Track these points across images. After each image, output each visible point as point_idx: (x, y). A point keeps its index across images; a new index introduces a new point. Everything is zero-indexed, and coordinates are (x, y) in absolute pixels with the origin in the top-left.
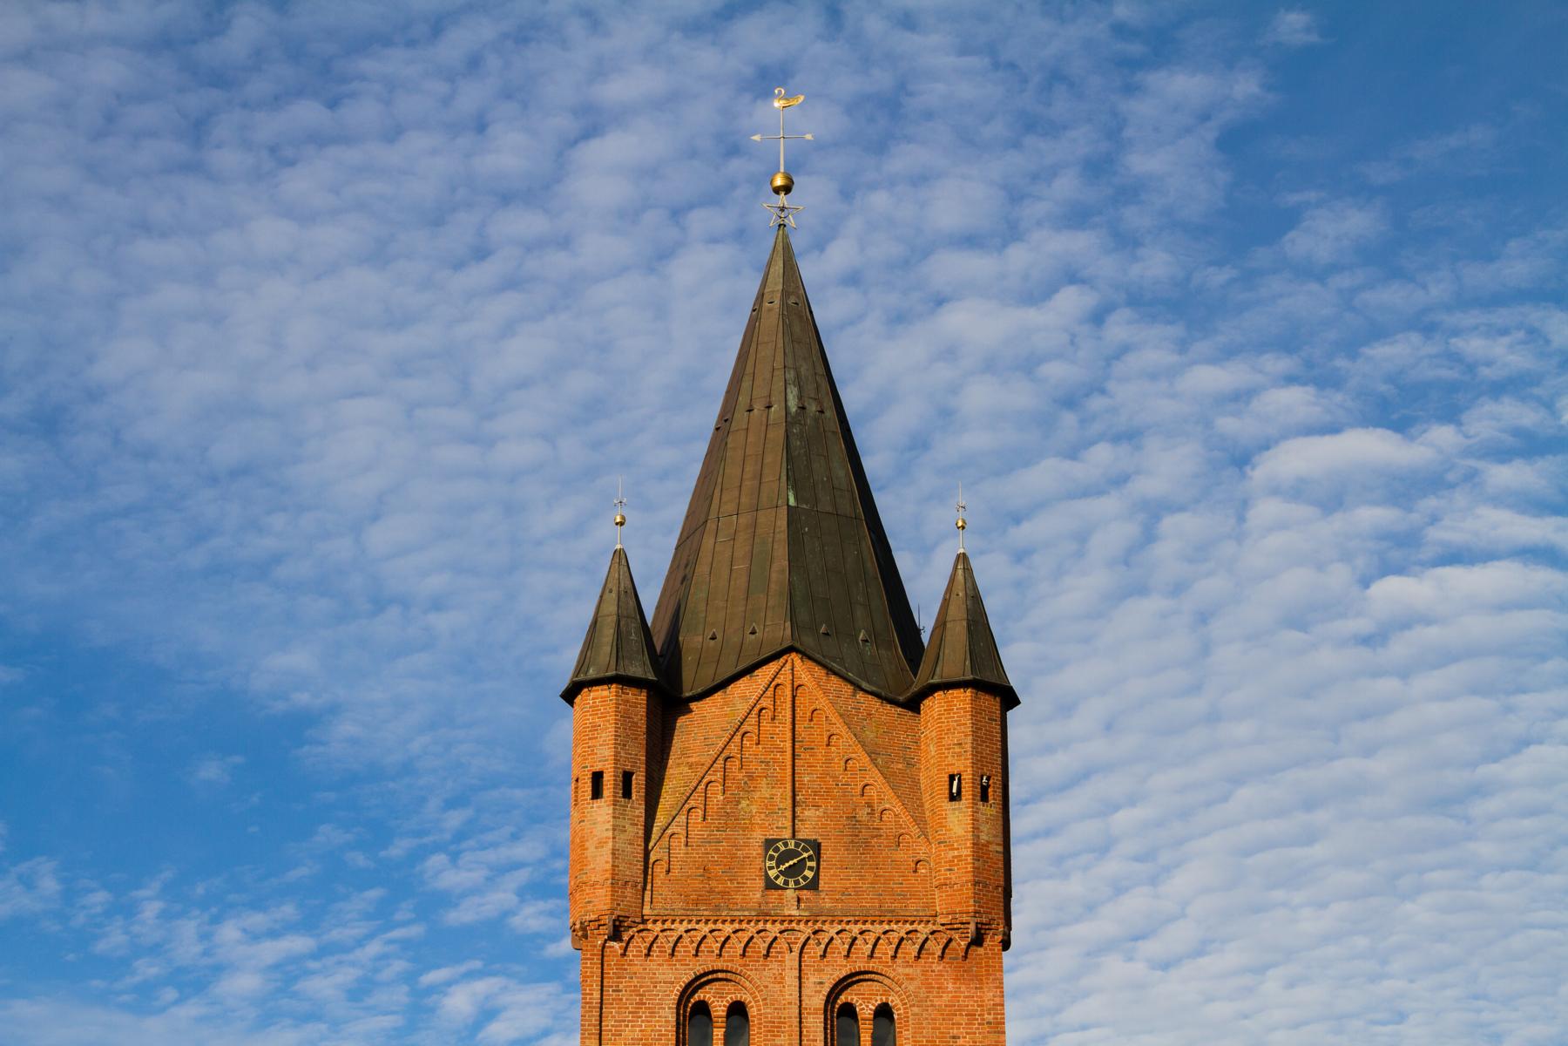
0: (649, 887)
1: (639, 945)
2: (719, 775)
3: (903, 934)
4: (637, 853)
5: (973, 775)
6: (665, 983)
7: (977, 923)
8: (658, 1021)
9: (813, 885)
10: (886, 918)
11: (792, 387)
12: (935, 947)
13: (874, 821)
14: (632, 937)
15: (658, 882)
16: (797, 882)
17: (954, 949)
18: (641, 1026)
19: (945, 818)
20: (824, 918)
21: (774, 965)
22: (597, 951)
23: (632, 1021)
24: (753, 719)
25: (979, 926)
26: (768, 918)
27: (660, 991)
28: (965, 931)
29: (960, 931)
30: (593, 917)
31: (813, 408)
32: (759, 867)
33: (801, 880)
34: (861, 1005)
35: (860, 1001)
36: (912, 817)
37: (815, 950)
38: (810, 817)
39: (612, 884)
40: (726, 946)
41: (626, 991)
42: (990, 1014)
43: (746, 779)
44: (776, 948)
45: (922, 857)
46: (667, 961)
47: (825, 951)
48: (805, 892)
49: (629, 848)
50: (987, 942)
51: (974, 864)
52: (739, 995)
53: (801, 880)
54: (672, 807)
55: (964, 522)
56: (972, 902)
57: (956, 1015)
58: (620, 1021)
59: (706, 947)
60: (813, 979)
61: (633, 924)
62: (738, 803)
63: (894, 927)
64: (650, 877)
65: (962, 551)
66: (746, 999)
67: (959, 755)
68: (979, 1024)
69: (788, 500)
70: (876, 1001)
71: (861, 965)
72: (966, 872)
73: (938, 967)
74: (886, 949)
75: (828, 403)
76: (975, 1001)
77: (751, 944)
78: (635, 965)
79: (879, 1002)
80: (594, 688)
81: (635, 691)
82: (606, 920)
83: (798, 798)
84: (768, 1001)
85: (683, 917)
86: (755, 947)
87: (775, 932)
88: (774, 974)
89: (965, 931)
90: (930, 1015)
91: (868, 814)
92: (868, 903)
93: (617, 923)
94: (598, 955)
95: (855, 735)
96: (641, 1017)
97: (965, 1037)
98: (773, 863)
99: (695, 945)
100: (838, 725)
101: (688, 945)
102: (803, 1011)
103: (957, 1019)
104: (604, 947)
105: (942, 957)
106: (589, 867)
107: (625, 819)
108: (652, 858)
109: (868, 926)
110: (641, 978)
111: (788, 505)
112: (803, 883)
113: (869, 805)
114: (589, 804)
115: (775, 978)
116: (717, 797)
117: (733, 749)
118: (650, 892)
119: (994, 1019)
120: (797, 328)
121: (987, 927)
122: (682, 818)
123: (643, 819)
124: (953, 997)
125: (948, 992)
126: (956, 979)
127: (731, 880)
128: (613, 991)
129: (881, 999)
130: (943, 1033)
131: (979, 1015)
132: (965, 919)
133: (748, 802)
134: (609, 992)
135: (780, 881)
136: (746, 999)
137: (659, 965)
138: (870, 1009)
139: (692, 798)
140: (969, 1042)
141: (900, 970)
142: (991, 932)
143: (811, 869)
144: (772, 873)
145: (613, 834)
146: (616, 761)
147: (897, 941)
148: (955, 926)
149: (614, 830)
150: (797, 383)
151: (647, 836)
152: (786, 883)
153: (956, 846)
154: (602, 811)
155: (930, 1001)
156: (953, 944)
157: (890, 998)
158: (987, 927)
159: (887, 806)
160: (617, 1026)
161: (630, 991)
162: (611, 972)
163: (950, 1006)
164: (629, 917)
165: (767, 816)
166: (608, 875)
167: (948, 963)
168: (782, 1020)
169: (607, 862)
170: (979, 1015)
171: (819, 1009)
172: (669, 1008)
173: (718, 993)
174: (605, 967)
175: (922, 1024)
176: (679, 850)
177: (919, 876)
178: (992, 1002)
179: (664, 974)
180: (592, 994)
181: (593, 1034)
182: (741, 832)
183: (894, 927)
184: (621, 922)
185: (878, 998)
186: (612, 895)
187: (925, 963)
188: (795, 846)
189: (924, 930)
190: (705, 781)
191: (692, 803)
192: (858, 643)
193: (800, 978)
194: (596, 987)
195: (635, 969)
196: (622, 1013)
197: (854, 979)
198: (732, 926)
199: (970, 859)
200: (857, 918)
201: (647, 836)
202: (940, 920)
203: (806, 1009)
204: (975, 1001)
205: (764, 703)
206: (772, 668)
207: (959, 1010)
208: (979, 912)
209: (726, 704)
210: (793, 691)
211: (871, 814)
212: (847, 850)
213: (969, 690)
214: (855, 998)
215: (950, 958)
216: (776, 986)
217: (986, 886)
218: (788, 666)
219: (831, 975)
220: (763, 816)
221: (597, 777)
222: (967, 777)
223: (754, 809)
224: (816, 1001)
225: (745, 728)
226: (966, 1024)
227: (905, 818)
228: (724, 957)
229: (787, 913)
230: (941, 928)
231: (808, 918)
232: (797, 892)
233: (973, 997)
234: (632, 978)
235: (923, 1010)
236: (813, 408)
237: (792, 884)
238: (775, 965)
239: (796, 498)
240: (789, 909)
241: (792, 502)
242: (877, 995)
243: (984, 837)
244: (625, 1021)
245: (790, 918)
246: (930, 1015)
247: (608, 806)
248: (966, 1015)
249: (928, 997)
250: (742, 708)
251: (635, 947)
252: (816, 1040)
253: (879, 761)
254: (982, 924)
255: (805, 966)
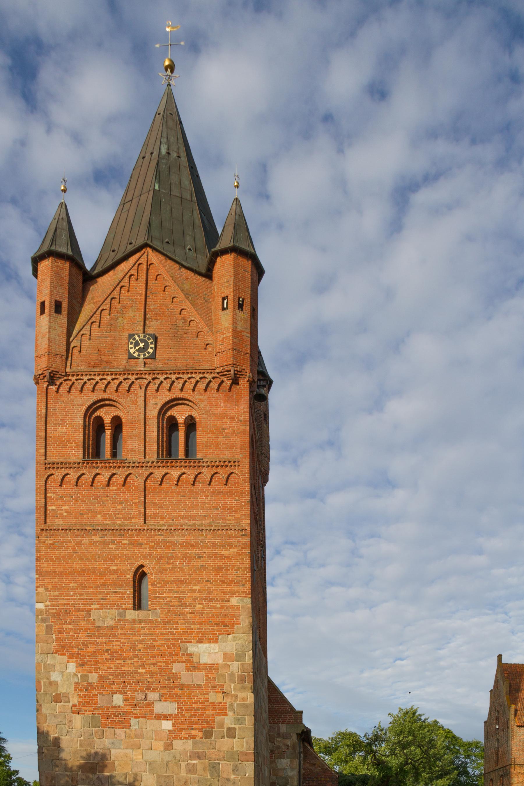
0: (70, 359)
1: (65, 387)
2: (107, 307)
3: (198, 378)
4: (63, 341)
5: (234, 296)
6: (78, 405)
7: (235, 370)
8: (75, 424)
9: (153, 356)
10: (189, 371)
11: (164, 145)
12: (214, 385)
13: (186, 326)
14: (61, 383)
15: (74, 357)
16: (144, 355)
17: (224, 387)
18: (66, 426)
19: (220, 319)
20: (158, 372)
21: (132, 396)
22: (44, 390)
23: (62, 424)
24: (126, 279)
25: (236, 372)
26: (129, 372)
27: (76, 409)
28: (229, 376)
29: (227, 376)
30: (40, 372)
31: (174, 155)
32: (126, 349)
33: (146, 354)
34: (178, 416)
35: (178, 415)
36: (205, 323)
37: (153, 387)
38: (153, 325)
39: (48, 354)
40: (109, 387)
41: (59, 410)
42: (242, 417)
43: (121, 308)
44: (134, 387)
45: (209, 342)
46: (79, 395)
47: (158, 388)
48: (149, 360)
49: (58, 338)
50: (241, 382)
51: (233, 340)
52: (117, 413)
53: (146, 354)
54: (83, 321)
55: (238, 183)
56: (231, 359)
57: (225, 418)
58: (56, 424)
59: (98, 388)
60: (152, 402)
61: (61, 377)
62: (117, 319)
63: (194, 375)
64: (70, 354)
65: (236, 197)
66: (120, 415)
67: (227, 287)
68: (236, 422)
69: (155, 186)
70: (186, 414)
71: (177, 395)
72: (229, 345)
73: (216, 395)
74: (189, 386)
75: (182, 148)
76: (234, 411)
77: (121, 386)
78: (63, 397)
79: (187, 415)
80: (42, 262)
81: (63, 262)
82: (47, 373)
83: (147, 316)
84: (129, 413)
85: (87, 373)
86: (123, 387)
87: (133, 379)
88: (133, 400)
89: (229, 376)
90: (212, 418)
91: (183, 323)
92: (180, 364)
93: (52, 375)
94: (44, 392)
95: (178, 286)
96: (66, 422)
97: (229, 429)
98: (132, 346)
99: (92, 386)
100: (169, 281)
101: (89, 386)
102: (147, 418)
103: (225, 420)
104: (47, 388)
105: (218, 390)
106: (39, 349)
107: (56, 323)
108: (72, 345)
109: (181, 376)
110: (66, 403)
111: (154, 189)
112: (147, 355)
113: (184, 319)
114: (39, 318)
115: (133, 402)
116: (106, 317)
117: (116, 294)
118: (70, 361)
119: (243, 419)
120: (170, 123)
121: (240, 373)
122: (88, 327)
123: (66, 325)
124: (223, 410)
125: (221, 407)
126: (225, 401)
127: (112, 355)
128: (53, 410)
129: (189, 414)
130: (218, 427)
131: (236, 418)
132: (228, 368)
133: (122, 319)
134: (50, 410)
135: (136, 355)
136: (120, 415)
137: (75, 397)
138: (183, 419)
139: (93, 317)
140: (231, 431)
141: (197, 397)
142: (243, 377)
143: (152, 348)
144: (132, 351)
145: (49, 330)
146: (51, 294)
147: (195, 382)
148: (224, 373)
149: (49, 328)
150: (167, 144)
151: (69, 334)
152: (139, 355)
153: (224, 332)
154: (45, 320)
155: (212, 412)
156: (224, 384)
157: (193, 413)
158: (240, 373)
159: (193, 319)
160: (54, 426)
161: (61, 410)
162: (50, 401)
163: (222, 414)
164: (58, 372)
165: (131, 325)
166: (47, 351)
167: (221, 393)
168: (136, 422)
169: (46, 344)
170: (236, 418)
171: (155, 417)
172: (80, 417)
173: (107, 412)
174: (49, 398)
175: (207, 423)
176: (86, 342)
177: (208, 352)
178: (242, 411)
179: (77, 401)
180: (42, 411)
181: (42, 430)
182: (118, 333)
183: (194, 375)
184: (54, 374)
185: (187, 413)
186: (48, 360)
187: (210, 393)
188: (144, 337)
189: (209, 377)
190: (100, 309)
191: (93, 319)
192: (185, 250)
193: (145, 401)
194: (44, 407)
195: (63, 399)
196: (57, 420)
197: (174, 403)
198: (111, 377)
199: (231, 338)
200: (174, 371)
201: (69, 334)
202: (218, 370)
203: (149, 416)
204: (234, 411)
205: (133, 272)
206: (137, 255)
207: (227, 416)
208: (236, 365)
209: (114, 275)
210: (147, 266)
211: (184, 323)
212: (171, 340)
213: (233, 254)
214: (175, 413)
215: (223, 391)
216: (134, 406)
217: (239, 352)
218: (145, 254)
219: (161, 400)
220: (129, 325)
221: (43, 304)
222: (231, 297)
223: (125, 322)
224: (153, 412)
225: (122, 284)
226: (230, 422)
227: (202, 324)
228: (107, 392)
229: (138, 369)
230: (218, 376)
231: (150, 372)
232: (145, 360)
233: (234, 409)
234: (62, 403)
235: (208, 416)
236: (174, 155)
237: (142, 356)
238: (133, 396)
239: (159, 187)
240: (140, 367)
241: (157, 187)
242: (186, 412)
243: (239, 328)
244: (58, 424)
245: (140, 372)
246: (212, 418)
247: (47, 317)
248: (230, 418)
249: (210, 410)
250: (121, 275)
251: (63, 388)
252: (153, 432)
253: (190, 298)
254: (238, 371)
255: (148, 396)
